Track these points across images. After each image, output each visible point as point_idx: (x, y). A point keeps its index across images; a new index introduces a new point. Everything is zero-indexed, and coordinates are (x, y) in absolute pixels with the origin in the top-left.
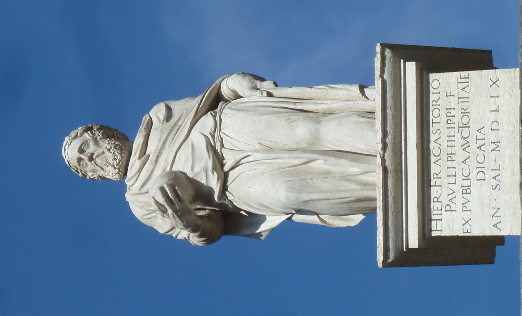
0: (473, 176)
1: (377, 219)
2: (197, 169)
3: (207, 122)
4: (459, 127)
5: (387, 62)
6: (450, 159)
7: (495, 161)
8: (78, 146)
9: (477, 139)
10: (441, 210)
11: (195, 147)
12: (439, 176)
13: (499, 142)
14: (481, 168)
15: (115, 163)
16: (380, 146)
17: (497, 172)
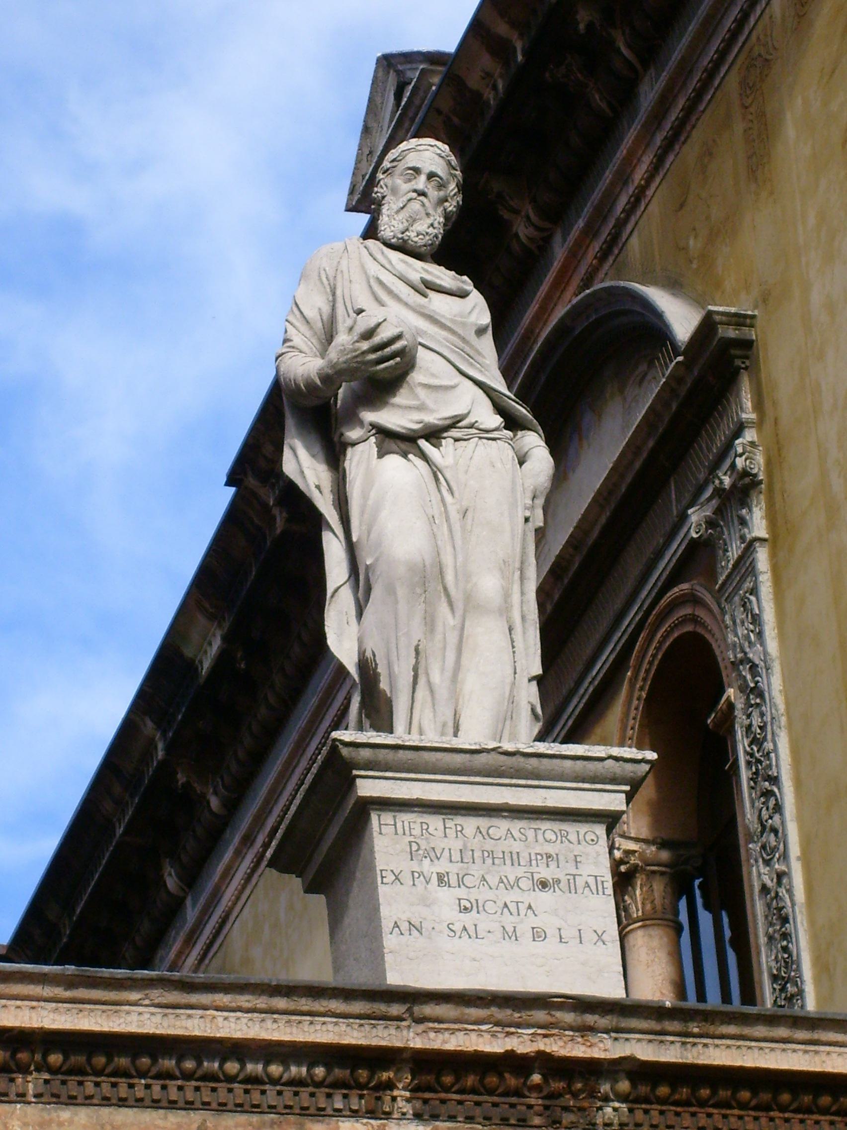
0: (462, 892)
2: (422, 393)
4: (532, 873)
5: (629, 767)
6: (486, 854)
8: (440, 173)
9: (517, 902)
12: (459, 833)
14: (477, 907)
17: (473, 934)
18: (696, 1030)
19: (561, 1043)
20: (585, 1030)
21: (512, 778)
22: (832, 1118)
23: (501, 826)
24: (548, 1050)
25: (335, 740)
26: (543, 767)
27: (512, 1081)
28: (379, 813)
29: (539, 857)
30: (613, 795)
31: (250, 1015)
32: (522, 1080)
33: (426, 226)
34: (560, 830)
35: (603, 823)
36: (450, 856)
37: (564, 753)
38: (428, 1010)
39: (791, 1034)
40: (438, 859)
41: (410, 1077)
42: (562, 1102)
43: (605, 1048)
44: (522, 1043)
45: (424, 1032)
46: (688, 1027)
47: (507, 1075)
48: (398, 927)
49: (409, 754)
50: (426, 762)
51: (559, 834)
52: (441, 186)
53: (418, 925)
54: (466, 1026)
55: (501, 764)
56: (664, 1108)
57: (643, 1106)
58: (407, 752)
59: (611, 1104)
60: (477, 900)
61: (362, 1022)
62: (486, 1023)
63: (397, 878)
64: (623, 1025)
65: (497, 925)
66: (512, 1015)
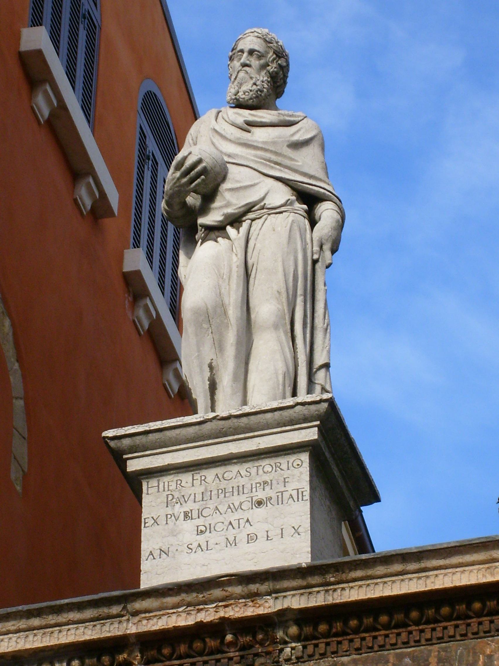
0: (200, 521)
1: (150, 424)
3: (280, 195)
4: (252, 497)
5: (313, 408)
6: (220, 491)
7: (217, 544)
8: (257, 48)
10: (169, 490)
11: (252, 188)
12: (203, 482)
13: (235, 545)
15: (240, 94)
16: (224, 414)
17: (204, 547)
18: (332, 579)
19: (237, 609)
20: (253, 596)
21: (234, 435)
22: (456, 622)
23: (233, 469)
24: (227, 616)
25: (105, 438)
26: (252, 422)
27: (212, 643)
28: (147, 480)
29: (258, 485)
30: (308, 430)
31: (18, 635)
32: (219, 641)
33: (250, 85)
34: (275, 463)
35: (304, 451)
36: (195, 499)
37: (263, 409)
38: (138, 605)
39: (404, 567)
40: (186, 502)
41: (139, 655)
42: (253, 651)
43: (269, 606)
44: (208, 615)
45: (139, 621)
46: (326, 579)
47: (207, 640)
48: (152, 555)
49: (157, 436)
50: (170, 438)
51: (274, 467)
52: (260, 57)
53: (166, 550)
54: (168, 611)
55: (222, 427)
56: (328, 640)
57: (314, 642)
58: (154, 434)
59: (290, 645)
60: (210, 524)
61: (95, 623)
62: (182, 606)
63: (155, 521)
64: (278, 587)
65: (224, 537)
66: (197, 597)
